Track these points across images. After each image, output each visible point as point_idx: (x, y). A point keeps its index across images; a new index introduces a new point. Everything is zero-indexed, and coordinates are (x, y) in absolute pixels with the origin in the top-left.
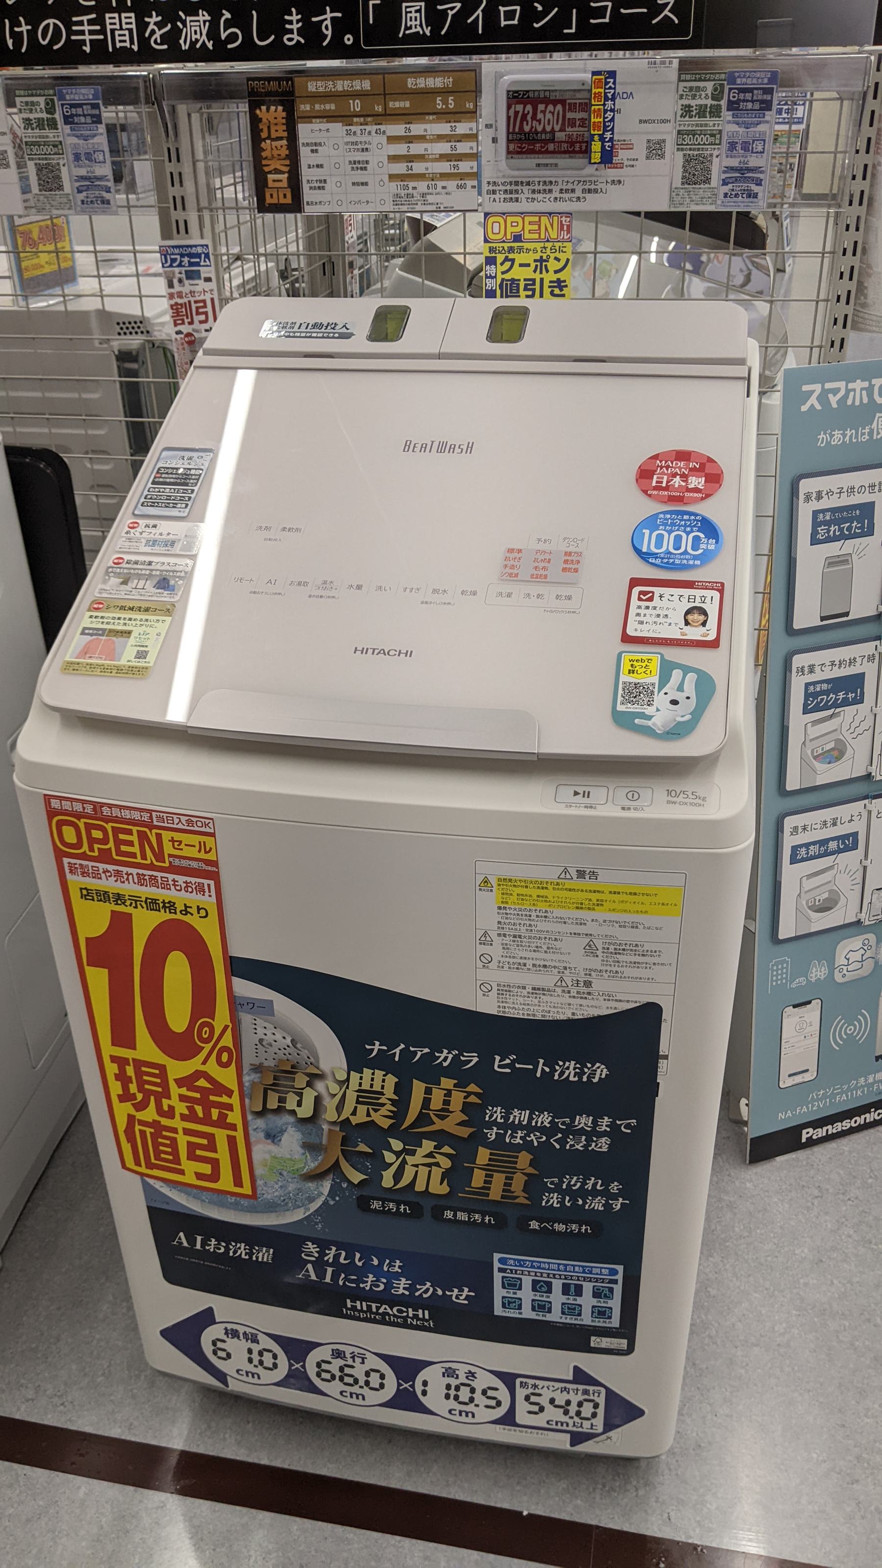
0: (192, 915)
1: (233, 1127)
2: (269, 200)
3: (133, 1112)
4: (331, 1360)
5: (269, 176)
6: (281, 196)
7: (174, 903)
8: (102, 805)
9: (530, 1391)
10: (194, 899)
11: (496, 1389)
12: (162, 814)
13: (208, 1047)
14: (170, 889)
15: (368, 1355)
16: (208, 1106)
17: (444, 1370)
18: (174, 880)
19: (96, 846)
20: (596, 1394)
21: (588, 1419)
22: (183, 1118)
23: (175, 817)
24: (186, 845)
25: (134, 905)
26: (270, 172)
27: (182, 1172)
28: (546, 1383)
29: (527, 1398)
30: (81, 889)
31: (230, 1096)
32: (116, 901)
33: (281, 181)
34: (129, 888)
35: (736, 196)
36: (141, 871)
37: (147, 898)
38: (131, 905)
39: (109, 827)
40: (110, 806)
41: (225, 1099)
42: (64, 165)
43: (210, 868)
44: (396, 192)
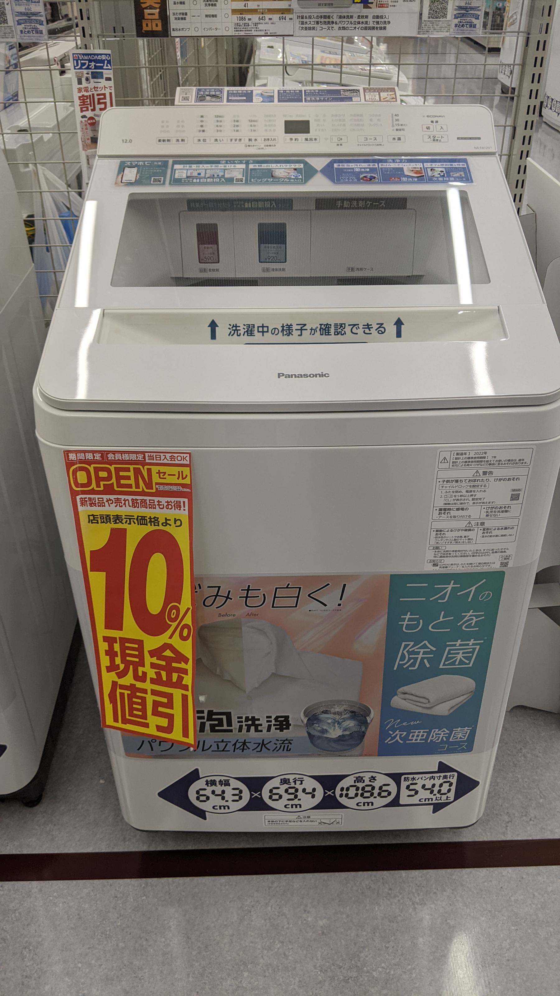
0: (170, 525)
1: (186, 688)
2: (145, 28)
3: (116, 679)
4: (280, 786)
5: (145, 10)
6: (154, 25)
7: (158, 518)
8: (108, 452)
9: (410, 782)
10: (172, 513)
11: (389, 785)
12: (152, 454)
13: (174, 625)
14: (155, 508)
15: (305, 777)
16: (170, 670)
17: (355, 779)
18: (159, 502)
19: (102, 483)
20: (451, 777)
21: (445, 794)
22: (153, 681)
23: (162, 454)
24: (169, 475)
25: (128, 522)
26: (146, 8)
27: (147, 725)
28: (420, 776)
29: (408, 787)
30: (89, 516)
31: (186, 663)
32: (116, 521)
33: (154, 14)
34: (125, 510)
35: (463, 26)
36: (134, 497)
37: (138, 516)
38: (126, 523)
39: (112, 468)
40: (114, 452)
41: (183, 665)
42: (8, 4)
43: (185, 490)
44: (237, 22)
